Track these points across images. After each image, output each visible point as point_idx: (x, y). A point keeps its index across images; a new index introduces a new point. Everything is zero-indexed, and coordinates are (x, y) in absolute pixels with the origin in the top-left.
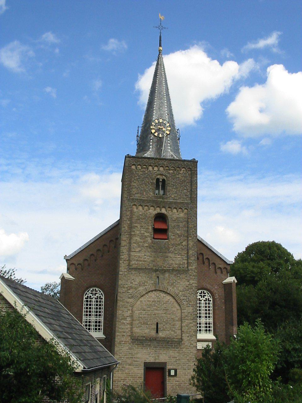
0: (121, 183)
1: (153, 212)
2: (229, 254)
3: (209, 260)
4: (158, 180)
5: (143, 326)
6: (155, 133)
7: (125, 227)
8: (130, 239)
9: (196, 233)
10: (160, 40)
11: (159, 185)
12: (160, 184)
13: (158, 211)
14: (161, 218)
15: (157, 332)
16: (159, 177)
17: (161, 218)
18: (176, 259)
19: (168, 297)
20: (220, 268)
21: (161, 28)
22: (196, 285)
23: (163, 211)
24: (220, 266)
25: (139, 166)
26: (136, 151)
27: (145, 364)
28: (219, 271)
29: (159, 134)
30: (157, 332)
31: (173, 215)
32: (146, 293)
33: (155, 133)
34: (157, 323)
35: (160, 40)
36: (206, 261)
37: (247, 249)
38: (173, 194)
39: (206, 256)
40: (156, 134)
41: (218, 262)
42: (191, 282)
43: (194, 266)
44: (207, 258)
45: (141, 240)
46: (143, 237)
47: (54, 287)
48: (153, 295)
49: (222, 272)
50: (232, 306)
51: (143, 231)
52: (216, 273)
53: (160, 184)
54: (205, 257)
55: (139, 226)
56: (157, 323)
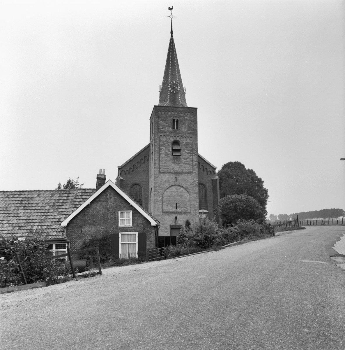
0: (149, 121)
1: (172, 140)
2: (218, 165)
3: (203, 166)
4: (174, 120)
5: (169, 205)
6: (171, 90)
7: (152, 149)
8: (160, 156)
9: (197, 151)
10: (172, 26)
11: (175, 123)
12: (176, 122)
13: (175, 139)
14: (176, 143)
15: (176, 208)
16: (174, 118)
17: (176, 143)
18: (186, 168)
19: (182, 189)
20: (210, 171)
21: (172, 17)
22: (198, 181)
23: (178, 139)
24: (210, 170)
25: (163, 112)
26: (158, 99)
27: (170, 226)
28: (209, 173)
29: (173, 91)
30: (176, 208)
31: (183, 141)
32: (169, 187)
33: (171, 90)
34: (176, 204)
35: (172, 26)
36: (202, 167)
37: (236, 162)
38: (184, 128)
39: (203, 165)
40: (172, 91)
41: (208, 167)
42: (195, 180)
43: (196, 171)
44: (202, 165)
45: (166, 156)
46: (167, 154)
47: (43, 217)
48: (173, 189)
49: (211, 174)
50: (217, 193)
51: (166, 150)
52: (208, 174)
53: (176, 122)
54: (201, 165)
55: (164, 148)
56: (176, 204)
